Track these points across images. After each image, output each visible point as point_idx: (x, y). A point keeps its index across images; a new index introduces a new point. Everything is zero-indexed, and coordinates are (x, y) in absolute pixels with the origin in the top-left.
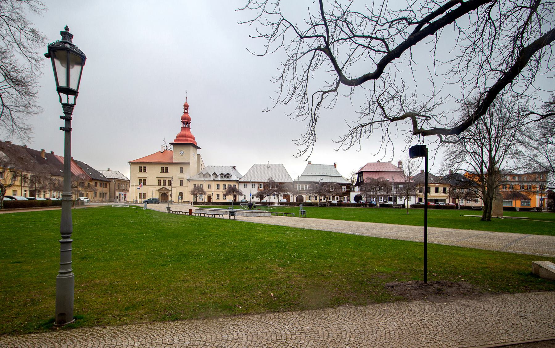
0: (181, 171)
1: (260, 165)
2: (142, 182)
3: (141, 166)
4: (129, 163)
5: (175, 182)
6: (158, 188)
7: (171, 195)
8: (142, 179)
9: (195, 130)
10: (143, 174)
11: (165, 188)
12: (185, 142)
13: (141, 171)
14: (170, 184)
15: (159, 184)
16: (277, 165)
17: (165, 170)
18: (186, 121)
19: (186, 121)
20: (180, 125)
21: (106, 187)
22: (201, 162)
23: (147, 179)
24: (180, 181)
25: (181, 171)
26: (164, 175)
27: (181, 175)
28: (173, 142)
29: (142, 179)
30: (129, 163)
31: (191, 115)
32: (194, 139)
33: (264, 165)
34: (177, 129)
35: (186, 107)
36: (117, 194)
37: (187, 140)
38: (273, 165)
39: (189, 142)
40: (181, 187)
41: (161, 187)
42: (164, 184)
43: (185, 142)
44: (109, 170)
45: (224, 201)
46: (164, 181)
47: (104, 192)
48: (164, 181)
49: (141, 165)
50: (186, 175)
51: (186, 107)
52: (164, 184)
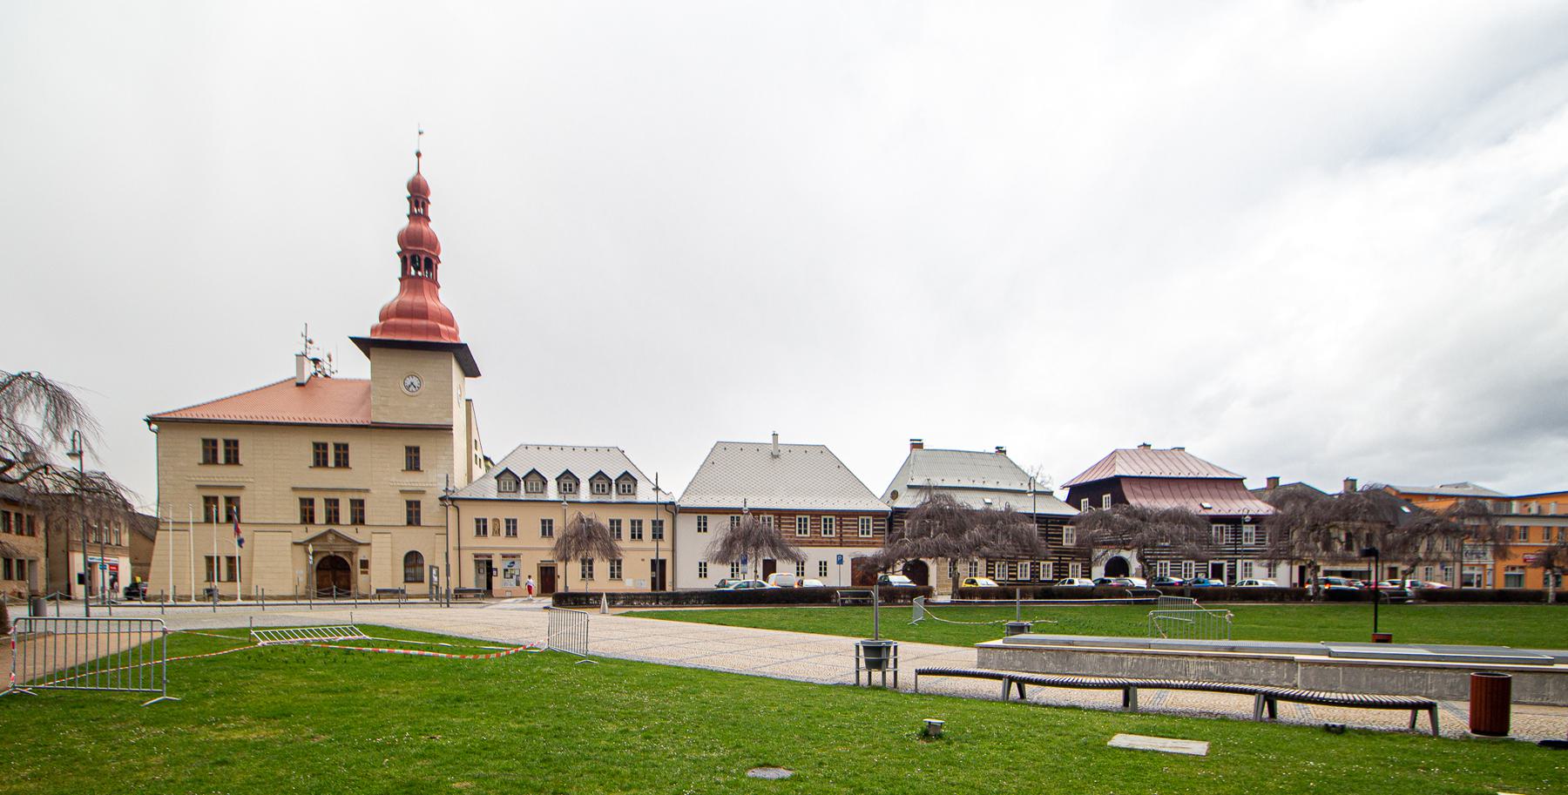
0: (413, 461)
1: (742, 447)
2: (223, 508)
4: (151, 420)
5: (385, 508)
7: (365, 564)
9: (454, 292)
10: (221, 474)
11: (338, 536)
12: (414, 338)
13: (210, 458)
14: (358, 519)
15: (308, 517)
16: (806, 449)
18: (419, 257)
19: (419, 257)
21: (32, 534)
22: (475, 436)
23: (243, 496)
24: (409, 503)
25: (413, 461)
26: (331, 478)
27: (412, 481)
28: (366, 334)
30: (151, 420)
31: (439, 223)
32: (450, 321)
33: (758, 447)
34: (384, 284)
35: (418, 194)
36: (78, 563)
37: (437, 332)
38: (791, 448)
39: (447, 340)
40: (413, 530)
41: (314, 531)
42: (333, 517)
43: (414, 338)
46: (332, 505)
47: (31, 554)
48: (332, 505)
50: (431, 482)
51: (418, 194)
52: (333, 517)
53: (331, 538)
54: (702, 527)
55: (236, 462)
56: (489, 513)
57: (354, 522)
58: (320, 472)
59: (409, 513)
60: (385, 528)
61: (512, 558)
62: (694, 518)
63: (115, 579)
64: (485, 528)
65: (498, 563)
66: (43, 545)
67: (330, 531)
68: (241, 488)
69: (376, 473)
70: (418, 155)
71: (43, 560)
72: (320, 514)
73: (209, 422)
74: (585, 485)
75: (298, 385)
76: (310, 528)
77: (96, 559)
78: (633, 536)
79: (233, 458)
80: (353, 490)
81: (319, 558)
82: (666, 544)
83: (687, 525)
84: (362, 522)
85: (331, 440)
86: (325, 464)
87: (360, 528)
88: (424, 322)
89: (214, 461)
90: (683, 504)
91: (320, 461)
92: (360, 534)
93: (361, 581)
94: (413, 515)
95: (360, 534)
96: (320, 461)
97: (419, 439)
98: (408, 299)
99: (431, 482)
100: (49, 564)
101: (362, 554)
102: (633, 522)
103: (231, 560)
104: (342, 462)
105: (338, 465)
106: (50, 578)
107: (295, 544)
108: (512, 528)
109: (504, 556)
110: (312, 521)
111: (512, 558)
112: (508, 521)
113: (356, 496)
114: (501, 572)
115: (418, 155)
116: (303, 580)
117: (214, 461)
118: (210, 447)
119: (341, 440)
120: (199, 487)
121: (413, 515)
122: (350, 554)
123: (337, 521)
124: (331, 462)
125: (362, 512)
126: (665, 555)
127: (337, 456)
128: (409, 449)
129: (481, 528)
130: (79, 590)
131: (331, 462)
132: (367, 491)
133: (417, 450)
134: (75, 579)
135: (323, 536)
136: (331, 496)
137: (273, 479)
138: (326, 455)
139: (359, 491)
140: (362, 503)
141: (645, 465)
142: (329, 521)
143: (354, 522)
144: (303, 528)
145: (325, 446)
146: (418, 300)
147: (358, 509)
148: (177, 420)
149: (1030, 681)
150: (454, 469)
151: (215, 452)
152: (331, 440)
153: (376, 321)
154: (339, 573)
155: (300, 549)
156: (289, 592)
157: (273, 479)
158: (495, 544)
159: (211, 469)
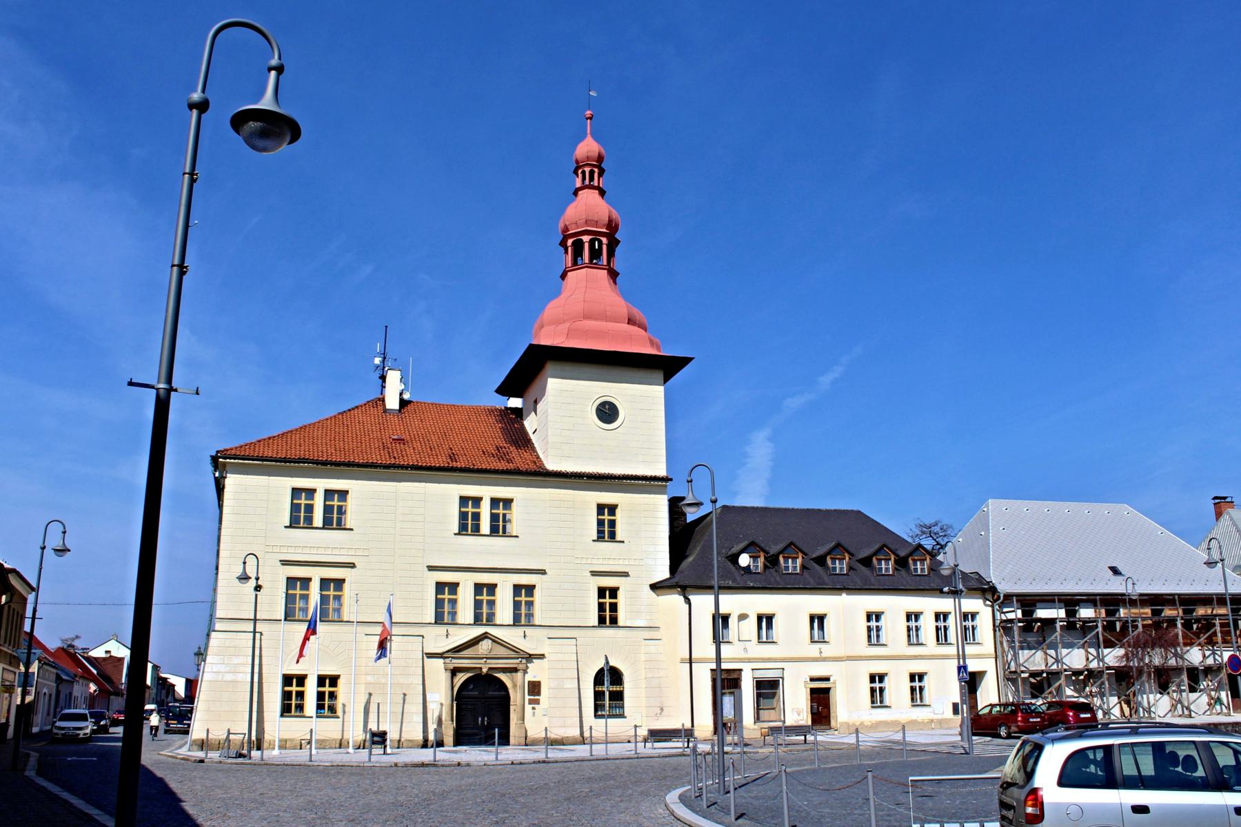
4: (282, 716)
5: (566, 599)
7: (535, 688)
11: (496, 641)
14: (523, 616)
15: (443, 615)
26: (483, 550)
27: (607, 556)
29: (316, 574)
40: (608, 632)
48: (485, 590)
59: (439, 603)
62: (723, 647)
67: (485, 636)
72: (466, 611)
74: (332, 689)
81: (461, 678)
86: (476, 530)
87: (529, 631)
103: (186, 732)
120: (595, 574)
123: (490, 620)
142: (478, 620)
143: (517, 621)
144: (442, 630)
149: (574, 742)
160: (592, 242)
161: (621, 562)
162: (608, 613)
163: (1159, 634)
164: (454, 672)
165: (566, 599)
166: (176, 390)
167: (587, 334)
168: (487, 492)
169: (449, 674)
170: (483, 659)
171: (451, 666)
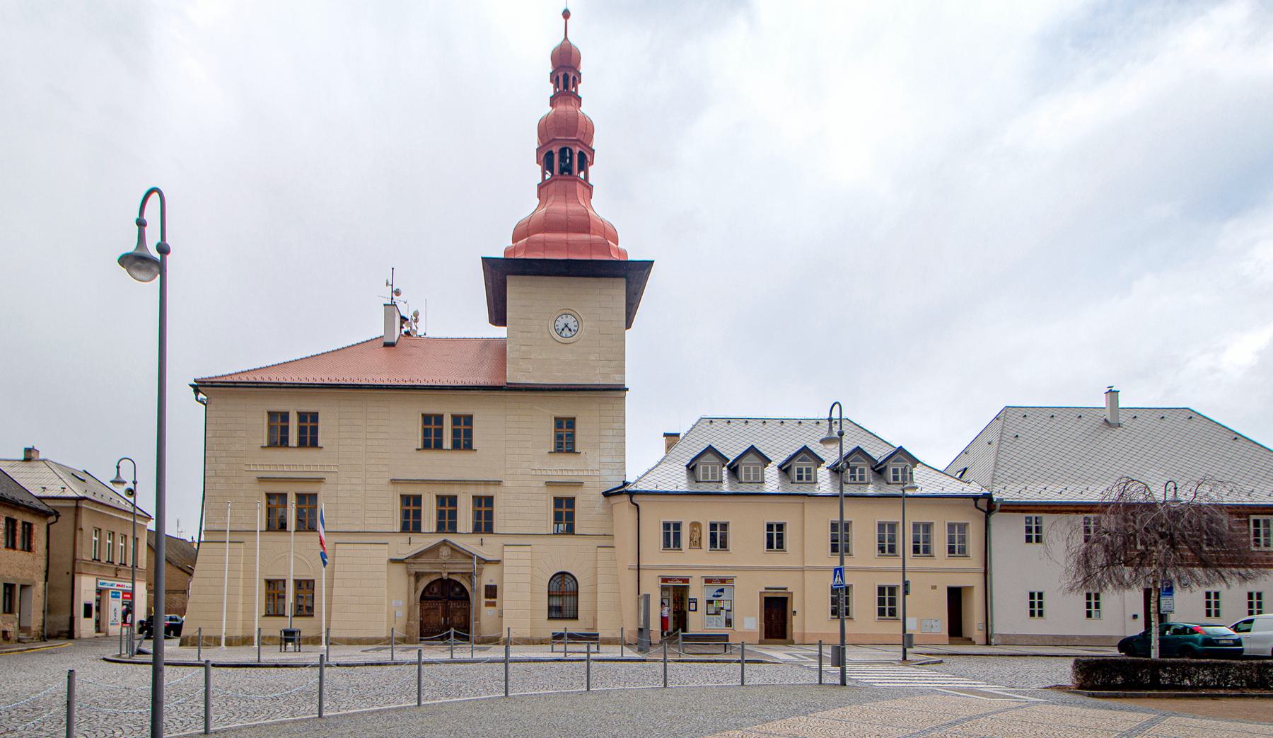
2: (291, 511)
3: (279, 406)
5: (525, 508)
6: (406, 546)
7: (492, 592)
8: (291, 491)
10: (293, 461)
11: (455, 550)
12: (567, 261)
13: (279, 440)
14: (484, 523)
15: (411, 523)
17: (446, 432)
18: (565, 153)
19: (565, 153)
20: (535, 173)
21: (28, 548)
23: (322, 491)
24: (406, 499)
26: (446, 465)
27: (564, 467)
29: (291, 491)
30: (665, 435)
31: (595, 99)
35: (566, 69)
36: (86, 588)
42: (447, 521)
43: (567, 261)
44: (30, 456)
45: (1037, 627)
46: (447, 505)
48: (447, 505)
49: (281, 410)
50: (589, 470)
51: (566, 69)
52: (447, 521)
53: (445, 551)
54: (1033, 535)
55: (314, 444)
56: (685, 514)
57: (477, 529)
58: (432, 456)
60: (523, 538)
61: (720, 583)
62: (1019, 520)
63: (129, 610)
64: (677, 537)
65: (697, 591)
66: (43, 564)
67: (445, 543)
68: (320, 480)
69: (511, 455)
70: (566, 14)
71: (40, 585)
73: (279, 386)
75: (386, 345)
76: (416, 538)
77: (108, 584)
78: (951, 550)
79: (309, 439)
80: (477, 483)
81: (424, 583)
82: (974, 560)
83: (1008, 531)
84: (489, 529)
85: (447, 408)
86: (439, 446)
87: (487, 539)
88: (585, 237)
89: (284, 443)
90: (642, 487)
91: (279, 440)
92: (485, 547)
93: (485, 617)
94: (564, 512)
95: (485, 547)
96: (431, 441)
97: (580, 404)
98: (559, 207)
99: (589, 470)
100: (49, 589)
101: (488, 576)
102: (951, 527)
104: (463, 441)
105: (456, 446)
106: (49, 610)
107: (393, 561)
108: (719, 538)
109: (708, 581)
110: (417, 528)
111: (720, 583)
112: (713, 526)
113: (482, 491)
114: (702, 605)
115: (566, 14)
116: (402, 614)
117: (284, 443)
118: (279, 423)
119: (308, 407)
121: (564, 512)
122: (470, 576)
123: (453, 528)
124: (447, 442)
125: (490, 515)
126: (973, 581)
127: (456, 433)
128: (559, 422)
129: (672, 535)
130: (85, 626)
131: (447, 442)
132: (498, 483)
133: (571, 422)
134: (80, 610)
135: (434, 549)
136: (446, 491)
137: (366, 466)
138: (439, 433)
139: (487, 483)
140: (489, 500)
141: (888, 424)
142: (440, 528)
143: (477, 529)
144: (405, 538)
145: (439, 419)
146: (572, 207)
147: (484, 506)
148: (235, 385)
150: (643, 453)
151: (285, 430)
152: (447, 408)
153: (510, 244)
154: (452, 605)
155: (400, 568)
156: (384, 634)
157: (366, 466)
158: (694, 562)
159: (279, 455)
160: (563, 151)
161: (266, 468)
162: (483, 521)
163: (1230, 560)
164: (418, 576)
165: (525, 508)
166: (1112, 394)
167: (545, 245)
168: (1033, 515)
169: (412, 579)
170: (447, 567)
171: (413, 571)
